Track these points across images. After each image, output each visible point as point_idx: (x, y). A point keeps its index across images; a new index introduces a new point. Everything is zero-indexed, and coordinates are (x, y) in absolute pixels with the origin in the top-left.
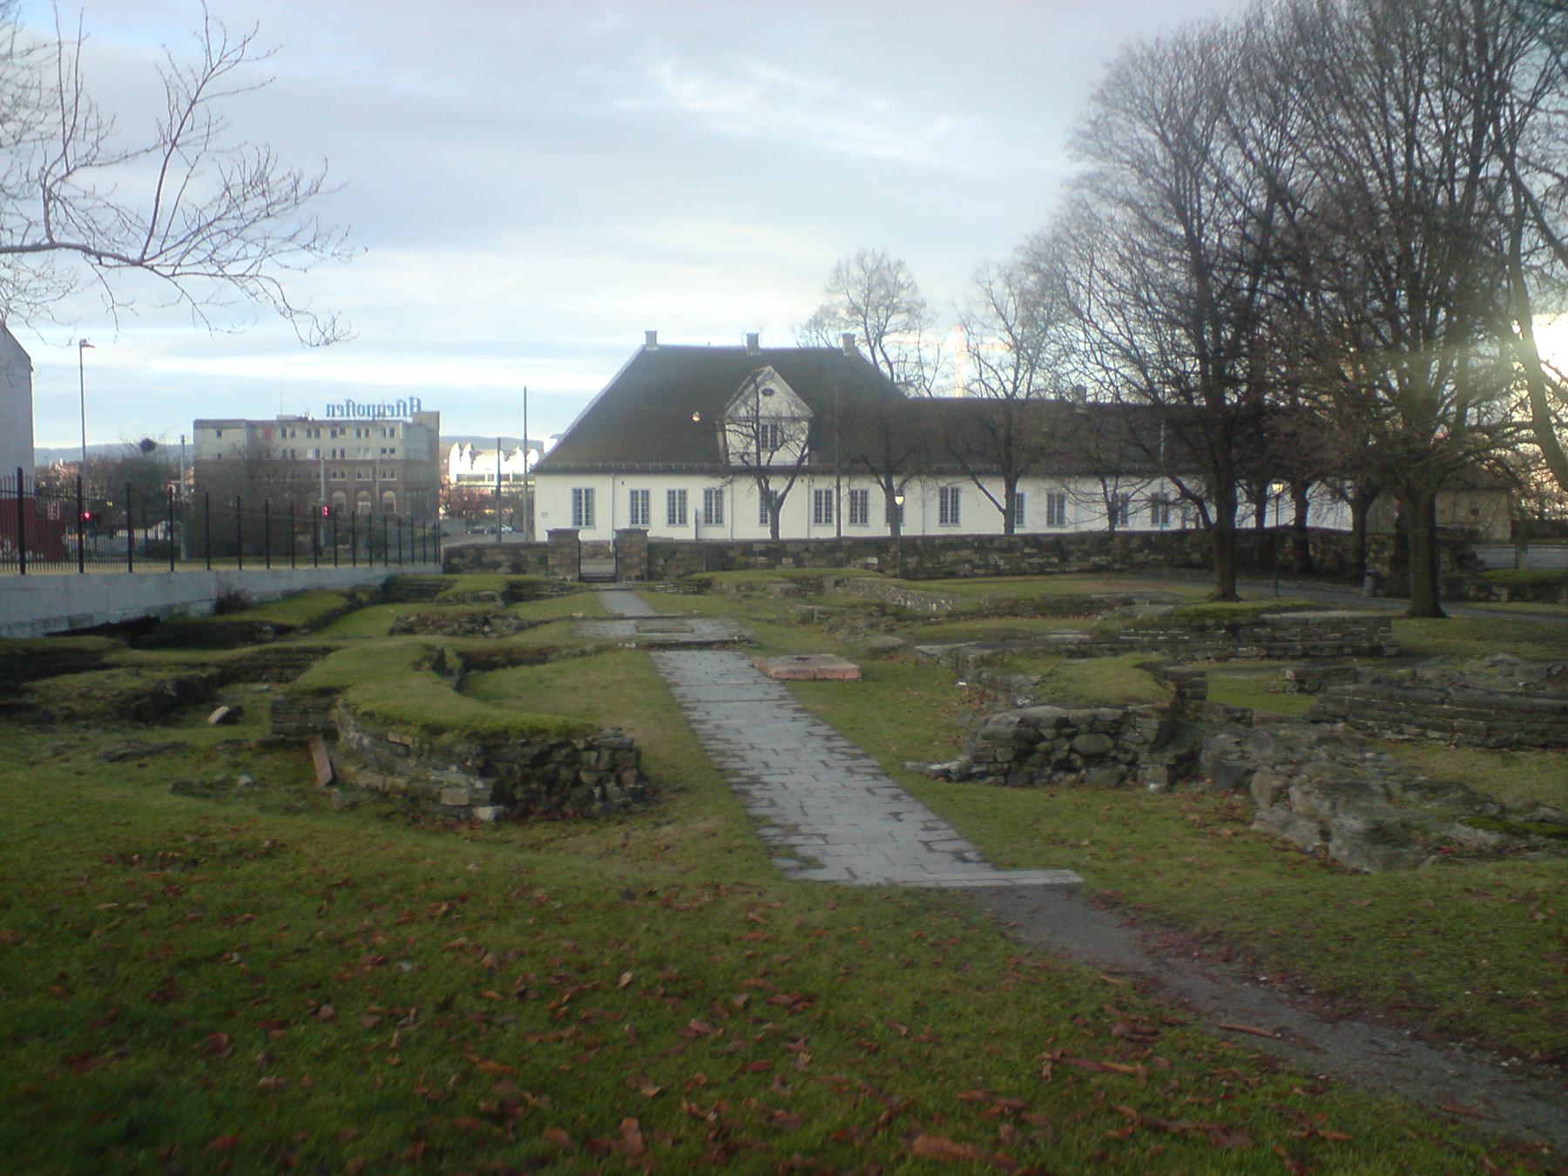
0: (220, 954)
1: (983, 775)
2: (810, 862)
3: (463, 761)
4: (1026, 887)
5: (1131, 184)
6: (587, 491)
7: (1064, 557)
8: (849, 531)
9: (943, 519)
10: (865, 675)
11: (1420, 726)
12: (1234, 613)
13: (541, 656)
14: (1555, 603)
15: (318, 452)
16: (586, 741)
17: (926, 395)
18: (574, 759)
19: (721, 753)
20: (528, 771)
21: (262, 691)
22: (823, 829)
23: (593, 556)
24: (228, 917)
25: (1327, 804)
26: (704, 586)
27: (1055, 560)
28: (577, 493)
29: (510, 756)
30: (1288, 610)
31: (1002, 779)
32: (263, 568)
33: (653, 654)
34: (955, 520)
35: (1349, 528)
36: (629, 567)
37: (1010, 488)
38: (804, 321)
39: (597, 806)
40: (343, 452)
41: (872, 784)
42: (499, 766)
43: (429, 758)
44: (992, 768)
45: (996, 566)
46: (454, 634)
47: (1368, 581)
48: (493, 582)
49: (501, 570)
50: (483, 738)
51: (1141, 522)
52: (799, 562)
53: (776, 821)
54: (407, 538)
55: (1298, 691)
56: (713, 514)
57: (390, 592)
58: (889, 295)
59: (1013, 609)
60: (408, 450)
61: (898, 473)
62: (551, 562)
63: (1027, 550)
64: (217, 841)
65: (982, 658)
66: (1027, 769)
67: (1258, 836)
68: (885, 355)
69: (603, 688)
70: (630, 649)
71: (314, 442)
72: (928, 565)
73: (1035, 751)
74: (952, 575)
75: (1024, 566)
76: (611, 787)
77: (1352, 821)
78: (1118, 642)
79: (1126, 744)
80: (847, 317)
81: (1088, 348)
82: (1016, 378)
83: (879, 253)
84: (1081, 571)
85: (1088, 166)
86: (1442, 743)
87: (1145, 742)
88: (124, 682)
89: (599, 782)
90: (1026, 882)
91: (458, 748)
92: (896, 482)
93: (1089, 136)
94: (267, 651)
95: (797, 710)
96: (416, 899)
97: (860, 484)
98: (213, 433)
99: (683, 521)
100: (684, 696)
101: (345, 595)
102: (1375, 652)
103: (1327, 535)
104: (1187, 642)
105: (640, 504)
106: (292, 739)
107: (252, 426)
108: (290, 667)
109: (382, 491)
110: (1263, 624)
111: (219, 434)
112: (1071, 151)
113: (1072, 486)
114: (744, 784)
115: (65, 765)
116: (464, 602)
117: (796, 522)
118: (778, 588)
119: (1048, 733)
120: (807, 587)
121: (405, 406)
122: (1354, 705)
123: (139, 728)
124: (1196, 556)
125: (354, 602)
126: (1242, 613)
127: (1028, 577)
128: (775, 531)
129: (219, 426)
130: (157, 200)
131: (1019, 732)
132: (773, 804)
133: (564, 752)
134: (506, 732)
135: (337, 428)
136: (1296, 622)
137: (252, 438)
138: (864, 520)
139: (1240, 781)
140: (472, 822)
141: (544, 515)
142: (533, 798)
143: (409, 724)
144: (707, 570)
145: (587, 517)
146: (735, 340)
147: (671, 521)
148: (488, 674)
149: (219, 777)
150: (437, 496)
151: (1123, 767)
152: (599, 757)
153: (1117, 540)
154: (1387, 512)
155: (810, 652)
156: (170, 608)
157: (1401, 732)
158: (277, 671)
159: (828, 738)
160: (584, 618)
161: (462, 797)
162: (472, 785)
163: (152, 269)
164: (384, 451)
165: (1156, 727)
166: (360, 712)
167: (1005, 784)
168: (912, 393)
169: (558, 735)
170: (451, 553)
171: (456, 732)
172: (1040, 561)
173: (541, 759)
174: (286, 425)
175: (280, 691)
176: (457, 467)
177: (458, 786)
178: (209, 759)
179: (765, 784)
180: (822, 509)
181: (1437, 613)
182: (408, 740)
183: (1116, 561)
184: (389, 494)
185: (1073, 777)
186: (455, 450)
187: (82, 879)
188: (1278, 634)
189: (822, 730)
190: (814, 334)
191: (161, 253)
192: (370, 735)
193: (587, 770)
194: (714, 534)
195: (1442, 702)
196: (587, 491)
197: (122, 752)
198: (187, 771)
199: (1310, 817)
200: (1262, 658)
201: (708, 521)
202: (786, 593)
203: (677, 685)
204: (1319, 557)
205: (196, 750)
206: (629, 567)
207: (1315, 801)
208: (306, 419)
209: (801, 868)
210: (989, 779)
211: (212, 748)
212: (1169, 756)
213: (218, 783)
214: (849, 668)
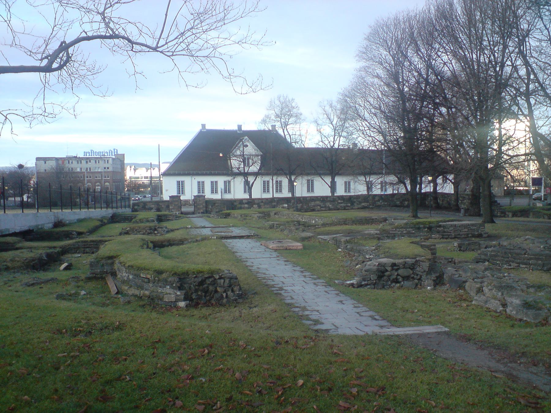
0: (120, 376)
1: (366, 285)
2: (317, 322)
3: (172, 284)
4: (428, 333)
5: (380, 71)
6: (182, 182)
7: (352, 204)
8: (277, 195)
9: (308, 191)
10: (304, 247)
11: (517, 263)
12: (430, 223)
13: (181, 242)
14: (528, 217)
15: (81, 169)
16: (219, 276)
17: (303, 147)
18: (214, 282)
19: (264, 278)
20: (197, 287)
21: (78, 257)
22: (317, 308)
23: (185, 205)
24: (116, 359)
25: (500, 294)
26: (227, 215)
27: (349, 205)
28: (178, 182)
29: (190, 282)
30: (448, 221)
31: (373, 286)
32: (69, 211)
33: (223, 241)
34: (313, 191)
35: (453, 192)
36: (199, 209)
37: (333, 179)
38: (260, 121)
39: (225, 301)
40: (90, 168)
41: (326, 289)
42: (185, 286)
43: (158, 283)
44: (369, 282)
45: (329, 207)
46: (144, 234)
47: (462, 211)
48: (152, 215)
49: (153, 211)
50: (179, 275)
51: (377, 191)
52: (259, 207)
53: (296, 305)
54: (114, 199)
55: (459, 250)
56: (227, 189)
57: (114, 219)
58: (290, 111)
59: (345, 222)
60: (113, 168)
61: (294, 174)
62: (171, 207)
63: (339, 201)
64: (95, 322)
65: (347, 240)
66: (382, 282)
67: (477, 306)
68: (288, 132)
69: (209, 254)
70: (214, 239)
71: (80, 165)
72: (305, 207)
73: (384, 276)
74: (313, 210)
75: (338, 207)
76: (230, 293)
77: (515, 300)
78: (389, 234)
79: (417, 272)
80: (274, 119)
81: (363, 129)
82: (334, 141)
83: (285, 95)
84: (358, 208)
85: (363, 64)
86: (526, 269)
87: (424, 271)
88: (26, 255)
89: (225, 292)
90: (428, 331)
91: (170, 279)
92: (293, 178)
93: (364, 53)
94: (79, 242)
95: (285, 261)
96: (191, 347)
97: (279, 179)
98: (43, 162)
99: (216, 192)
100: (240, 256)
101: (99, 220)
102: (480, 236)
103: (444, 195)
104: (414, 233)
105: (201, 186)
106: (98, 276)
107: (57, 159)
108: (87, 248)
109: (105, 182)
110: (440, 226)
111: (45, 163)
112: (357, 58)
113: (359, 178)
114: (277, 290)
115: (10, 288)
116: (143, 222)
117: (257, 193)
118: (256, 216)
119: (389, 269)
120: (266, 216)
121: (112, 152)
122: (491, 256)
123: (34, 272)
124: (398, 203)
125: (103, 223)
126: (433, 222)
127: (341, 211)
128: (250, 195)
129: (45, 160)
130: (166, 15)
131: (378, 268)
132: (292, 298)
133: (210, 280)
134: (187, 273)
135: (88, 160)
136: (452, 226)
137: (58, 164)
138: (281, 191)
139: (461, 285)
140: (178, 308)
141: (167, 190)
142: (199, 298)
143: (149, 270)
144: (227, 210)
145: (182, 191)
146: (235, 128)
147: (212, 192)
148: (162, 249)
149: (73, 292)
150: (124, 184)
151: (416, 281)
152: (224, 282)
153: (371, 197)
154: (467, 187)
155: (282, 239)
156: (37, 226)
157: (510, 265)
158: (83, 249)
159: (302, 272)
160: (191, 228)
161: (173, 298)
162: (176, 293)
163: (161, 52)
164: (105, 168)
165: (428, 265)
166: (127, 265)
167: (374, 288)
168: (297, 146)
169: (208, 273)
170: (134, 205)
171: (168, 273)
172: (344, 205)
173: (202, 283)
174: (69, 159)
175: (90, 258)
176: (129, 174)
177: (170, 294)
178: (66, 284)
179: (286, 290)
180: (266, 188)
181: (493, 222)
182: (149, 276)
183: (370, 205)
184: (107, 184)
185: (398, 285)
186: (128, 168)
187: (47, 342)
188: (446, 230)
189: (298, 268)
190: (263, 125)
191: (166, 43)
192: (132, 274)
193: (219, 287)
194: (228, 196)
195: (525, 254)
196: (182, 182)
197: (32, 282)
198: (60, 290)
199: (495, 298)
200: (441, 238)
201: (225, 192)
202: (259, 217)
203: (236, 252)
204: (441, 203)
205: (61, 281)
206: (199, 209)
207: (495, 293)
208: (76, 157)
209: (315, 324)
210: (368, 287)
211: (68, 280)
212: (434, 276)
213: (73, 294)
214: (299, 245)
